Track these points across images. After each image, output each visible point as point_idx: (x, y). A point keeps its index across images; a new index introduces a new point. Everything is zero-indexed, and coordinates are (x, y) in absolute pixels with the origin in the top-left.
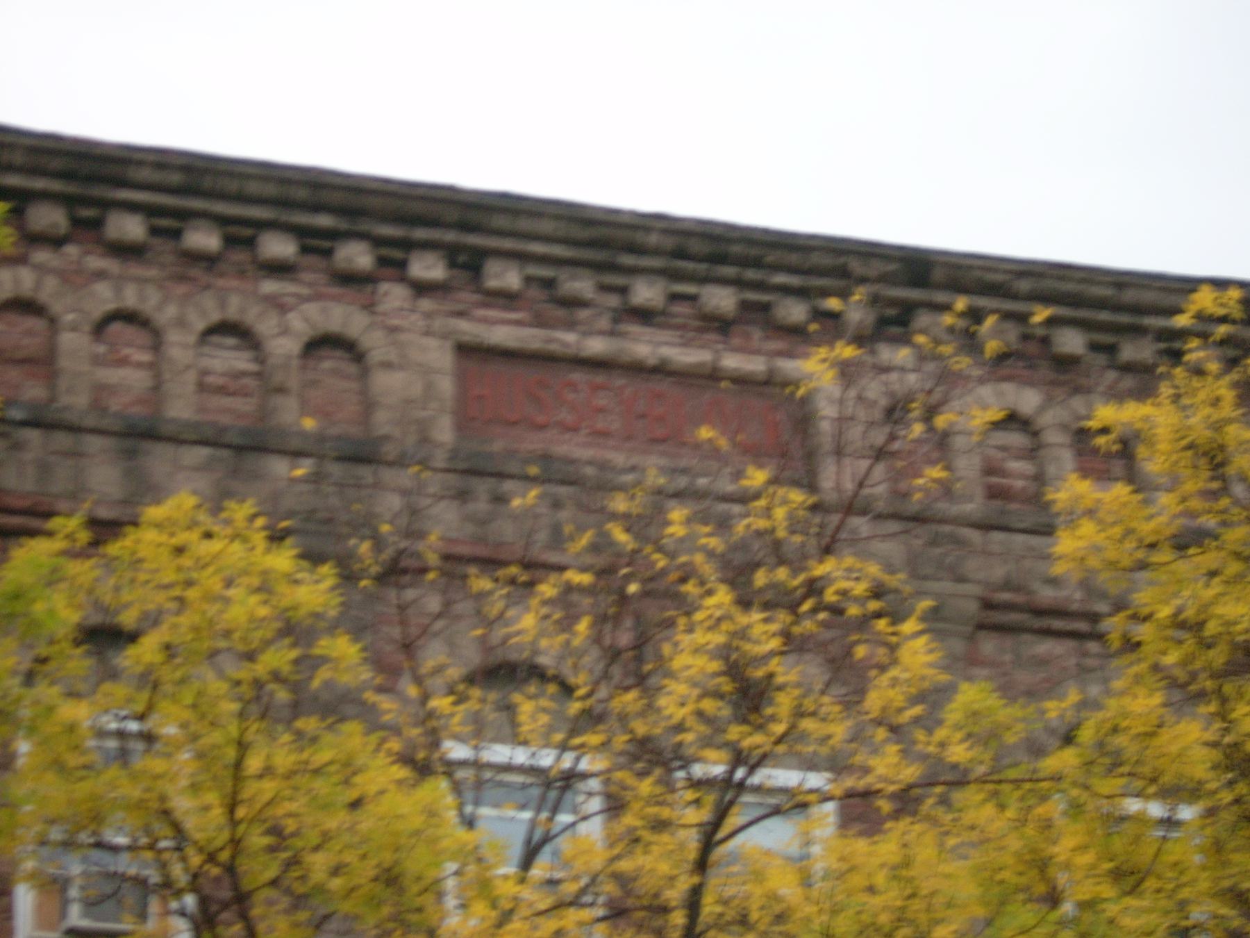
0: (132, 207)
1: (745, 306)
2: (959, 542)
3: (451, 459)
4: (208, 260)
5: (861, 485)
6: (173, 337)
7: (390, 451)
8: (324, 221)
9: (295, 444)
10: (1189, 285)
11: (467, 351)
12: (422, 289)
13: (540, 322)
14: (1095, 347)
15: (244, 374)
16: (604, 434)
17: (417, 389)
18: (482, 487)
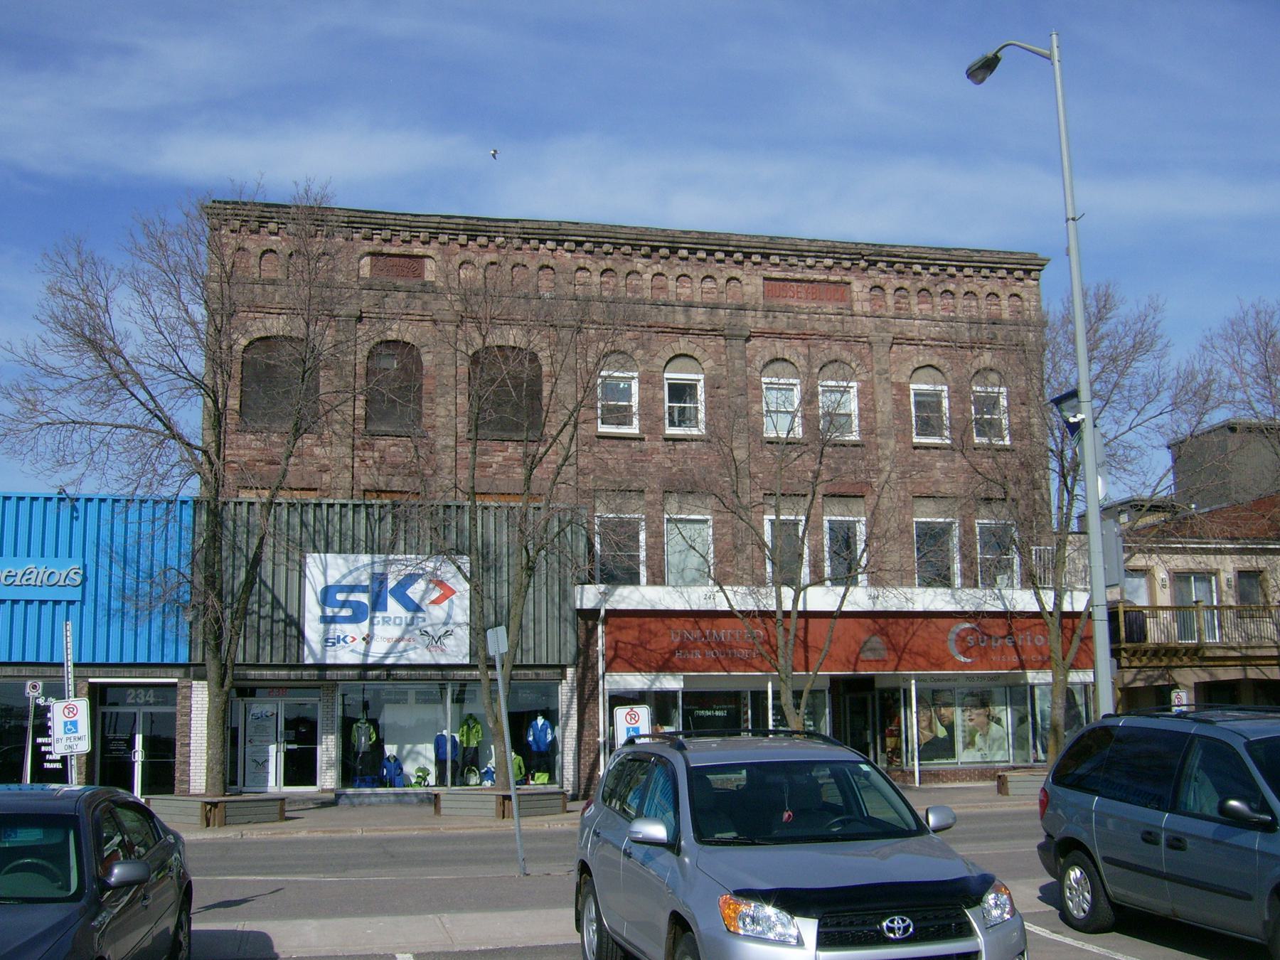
0: (685, 248)
2: (888, 322)
4: (704, 260)
5: (64, 326)
7: (748, 307)
8: (731, 249)
11: (765, 279)
13: (784, 271)
18: (771, 314)
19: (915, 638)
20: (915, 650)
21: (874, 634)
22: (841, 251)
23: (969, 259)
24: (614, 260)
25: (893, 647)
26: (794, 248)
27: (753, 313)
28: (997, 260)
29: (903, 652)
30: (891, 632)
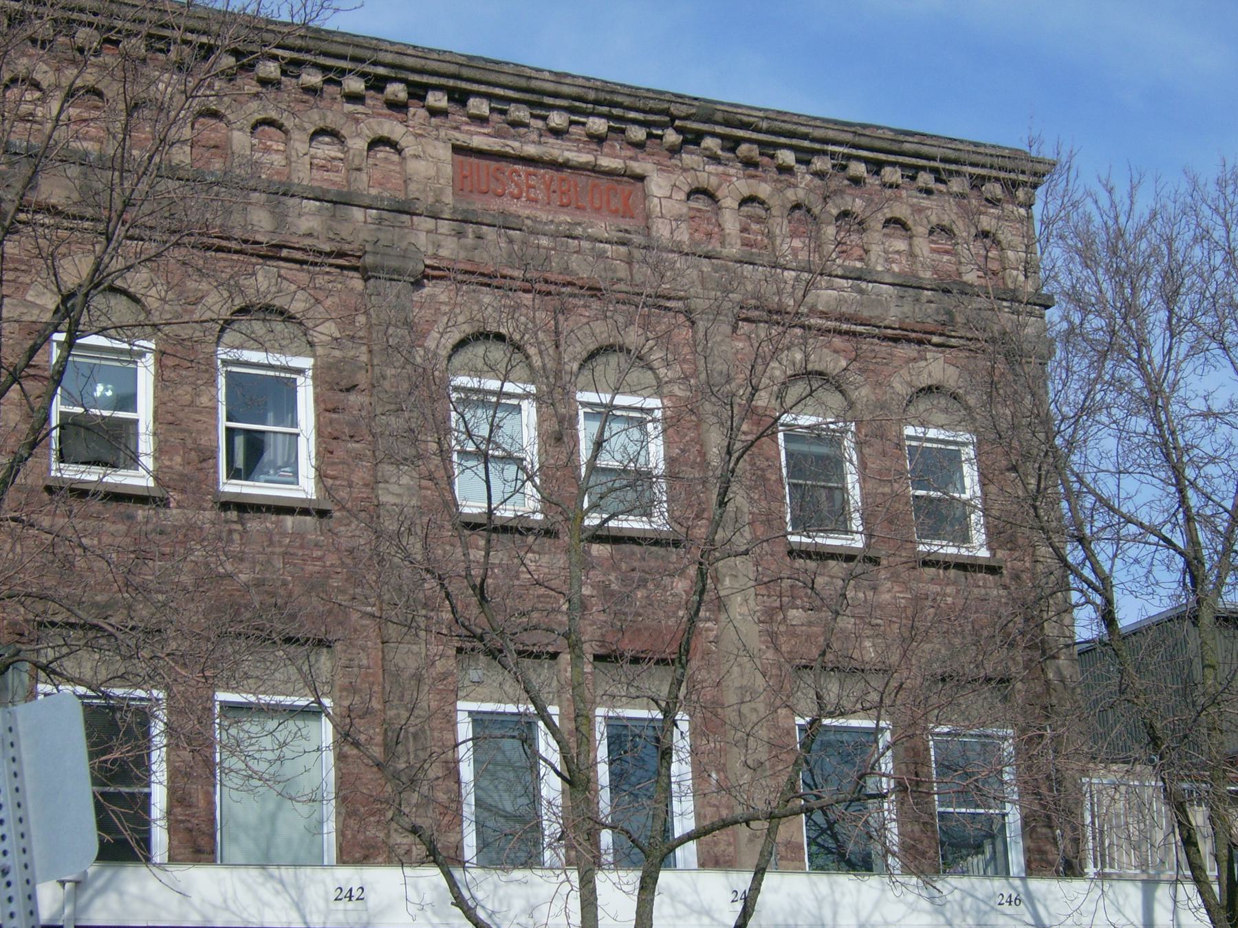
1: (610, 129)
3: (454, 212)
6: (296, 135)
8: (381, 71)
9: (367, 202)
10: (92, 774)
11: (458, 149)
12: (434, 112)
13: (498, 134)
14: (798, 161)
15: (334, 159)
16: (536, 201)
17: (432, 172)
18: (470, 229)
27: (430, 223)
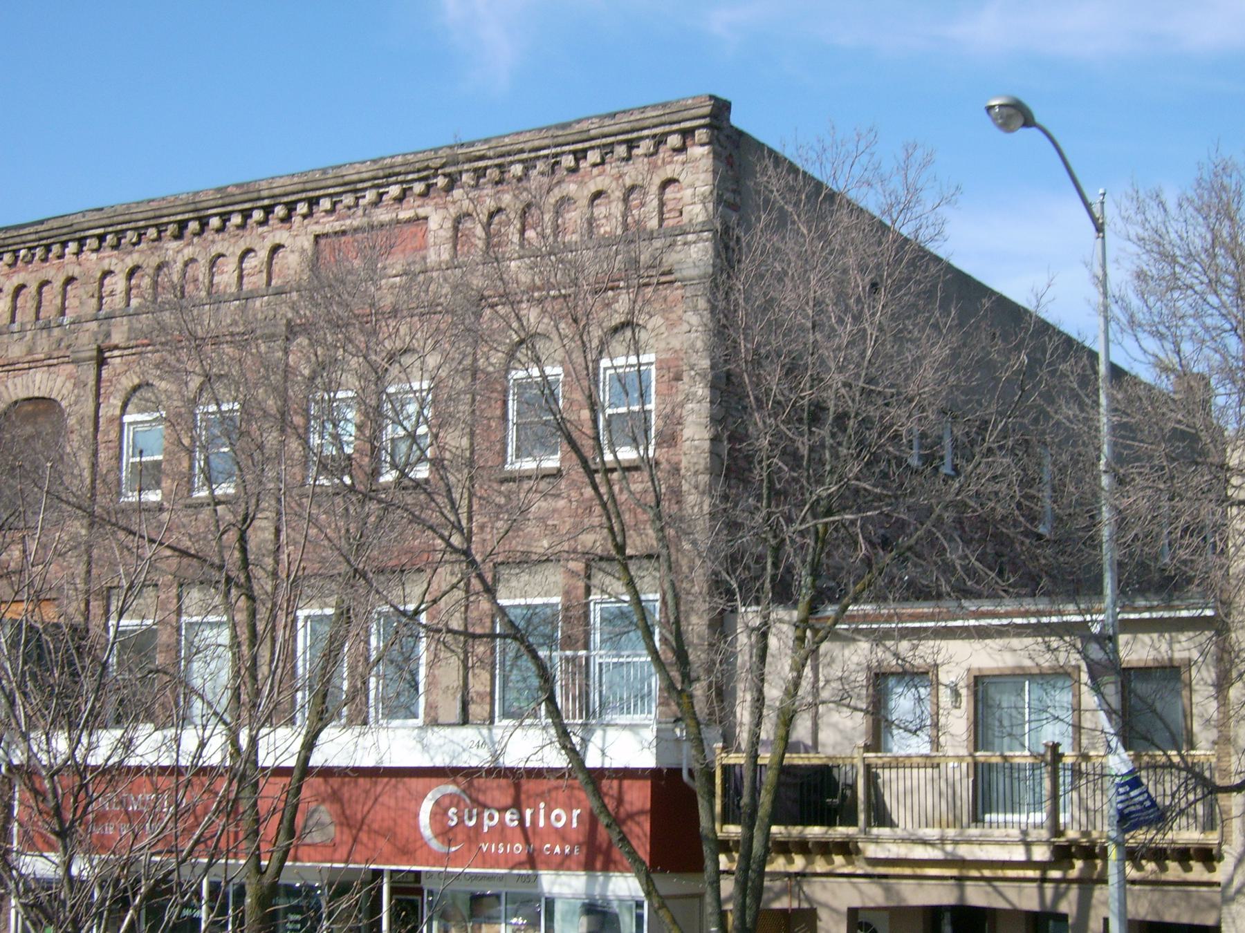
0: (215, 215)
7: (117, 313)
19: (378, 807)
20: (375, 826)
21: (324, 801)
22: (402, 169)
23: (584, 136)
24: (142, 252)
25: (345, 821)
26: (340, 181)
28: (627, 127)
29: (360, 829)
30: (346, 795)
